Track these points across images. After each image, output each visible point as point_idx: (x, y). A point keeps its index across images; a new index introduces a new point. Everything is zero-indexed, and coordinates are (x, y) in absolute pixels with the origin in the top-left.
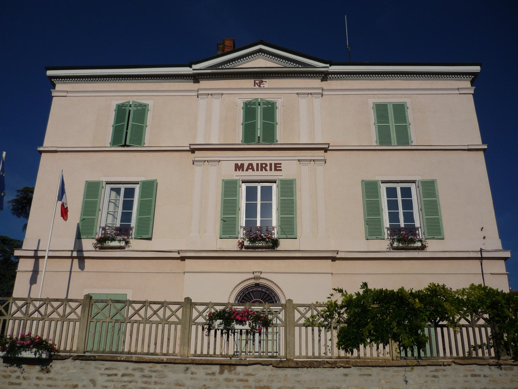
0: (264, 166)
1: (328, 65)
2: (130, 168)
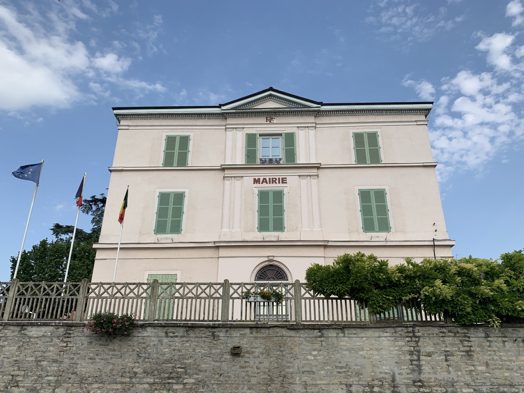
2: (174, 182)
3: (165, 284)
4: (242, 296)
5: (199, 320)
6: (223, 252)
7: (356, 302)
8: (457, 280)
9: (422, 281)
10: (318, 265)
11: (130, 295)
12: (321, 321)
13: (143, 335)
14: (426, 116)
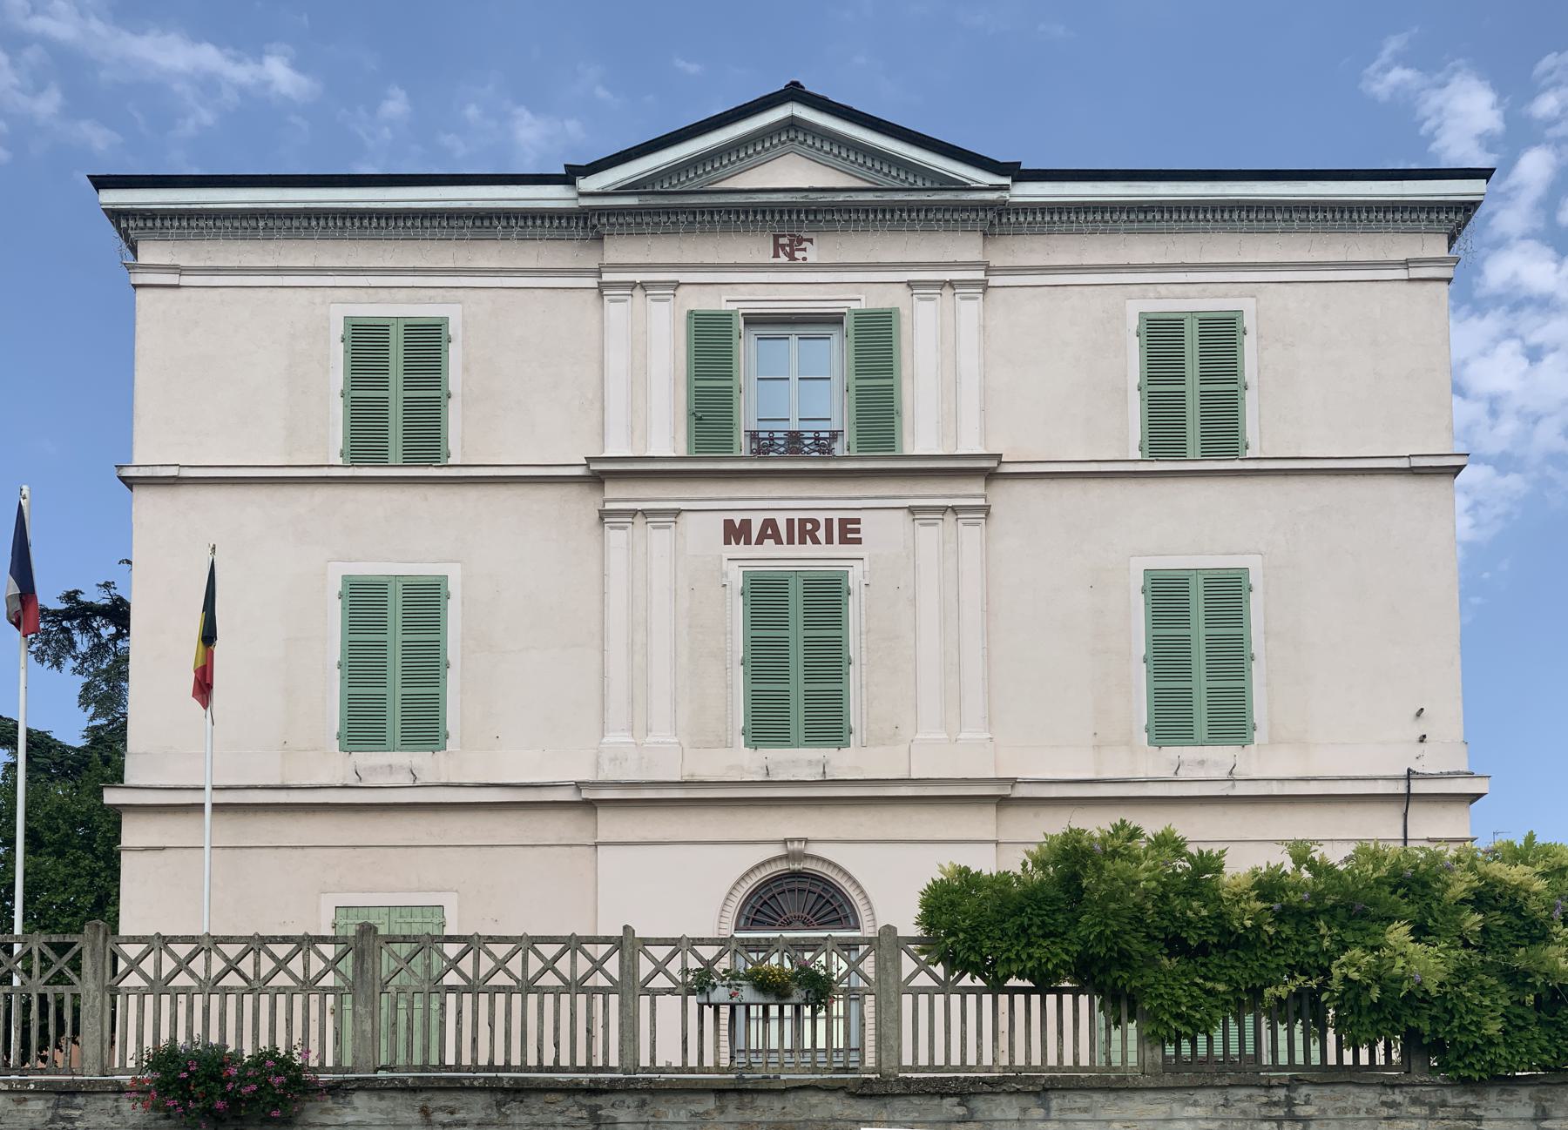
0: (809, 526)
1: (1007, 181)
2: (398, 533)
3: (405, 939)
4: (685, 984)
5: (540, 1068)
6: (611, 825)
7: (1097, 1001)
8: (1467, 924)
9: (1342, 926)
10: (967, 870)
11: (324, 982)
12: (970, 1069)
13: (340, 1120)
14: (1452, 239)
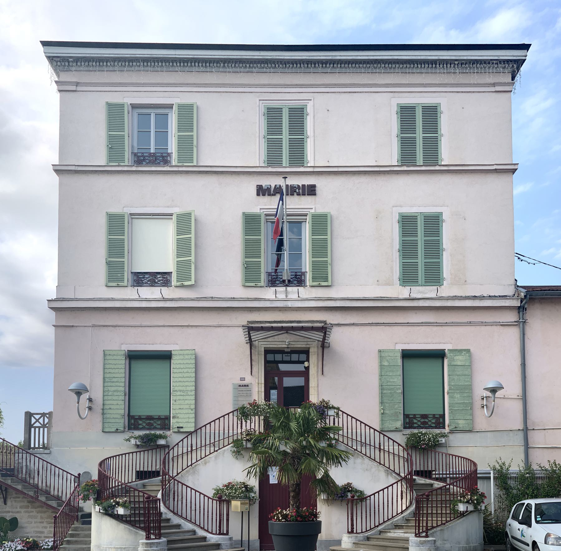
2: (418, 194)
